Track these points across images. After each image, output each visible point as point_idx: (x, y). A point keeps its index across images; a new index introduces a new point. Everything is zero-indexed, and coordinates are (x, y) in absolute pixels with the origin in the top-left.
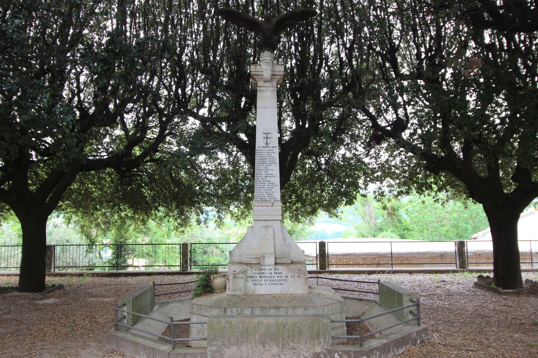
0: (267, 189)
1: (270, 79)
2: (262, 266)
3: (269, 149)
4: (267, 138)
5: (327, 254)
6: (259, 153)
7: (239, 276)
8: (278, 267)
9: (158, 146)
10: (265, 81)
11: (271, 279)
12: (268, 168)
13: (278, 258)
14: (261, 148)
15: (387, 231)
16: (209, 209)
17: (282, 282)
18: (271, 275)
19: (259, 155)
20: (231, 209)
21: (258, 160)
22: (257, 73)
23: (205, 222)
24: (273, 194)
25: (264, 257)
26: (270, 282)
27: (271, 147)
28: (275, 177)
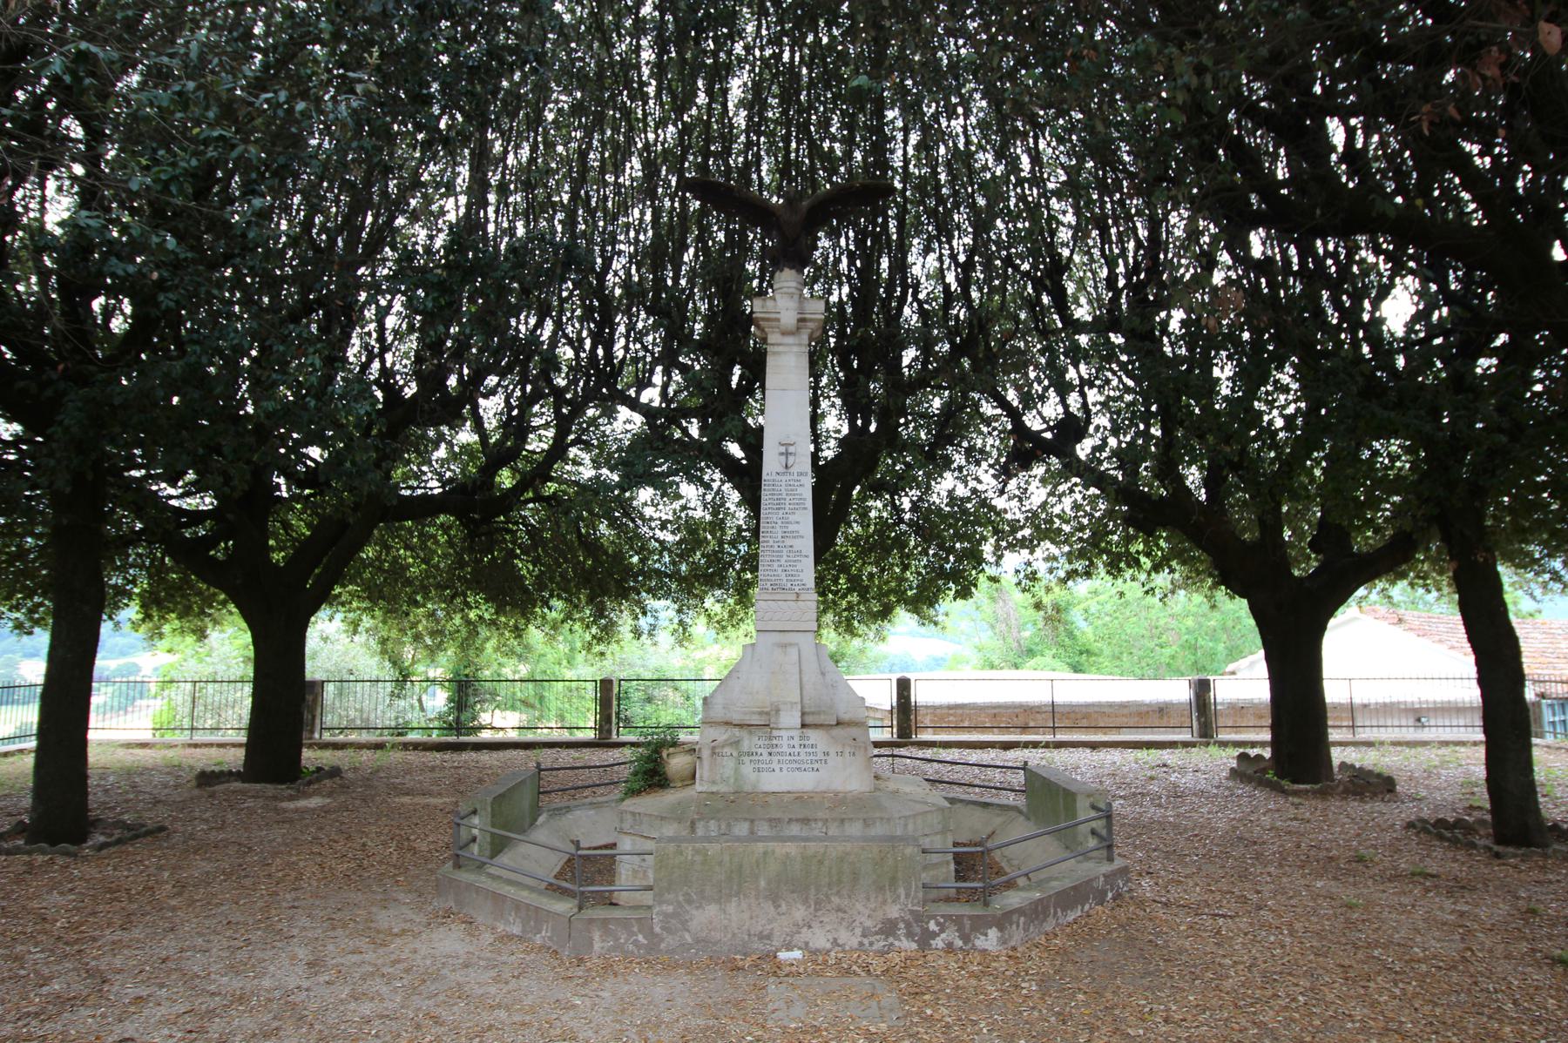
1: (794, 329)
4: (787, 454)
10: (784, 333)
11: (792, 758)
13: (809, 713)
14: (774, 477)
17: (816, 766)
18: (792, 750)
23: (650, 634)
25: (778, 711)
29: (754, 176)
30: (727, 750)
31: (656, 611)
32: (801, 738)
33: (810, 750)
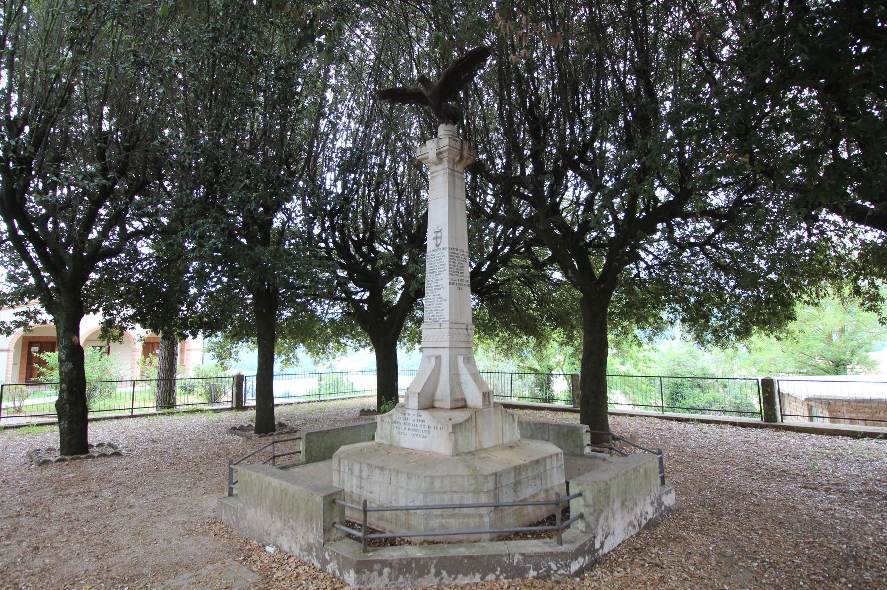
9: (509, 260)
11: (414, 428)
17: (425, 434)
29: (627, 68)
33: (421, 424)
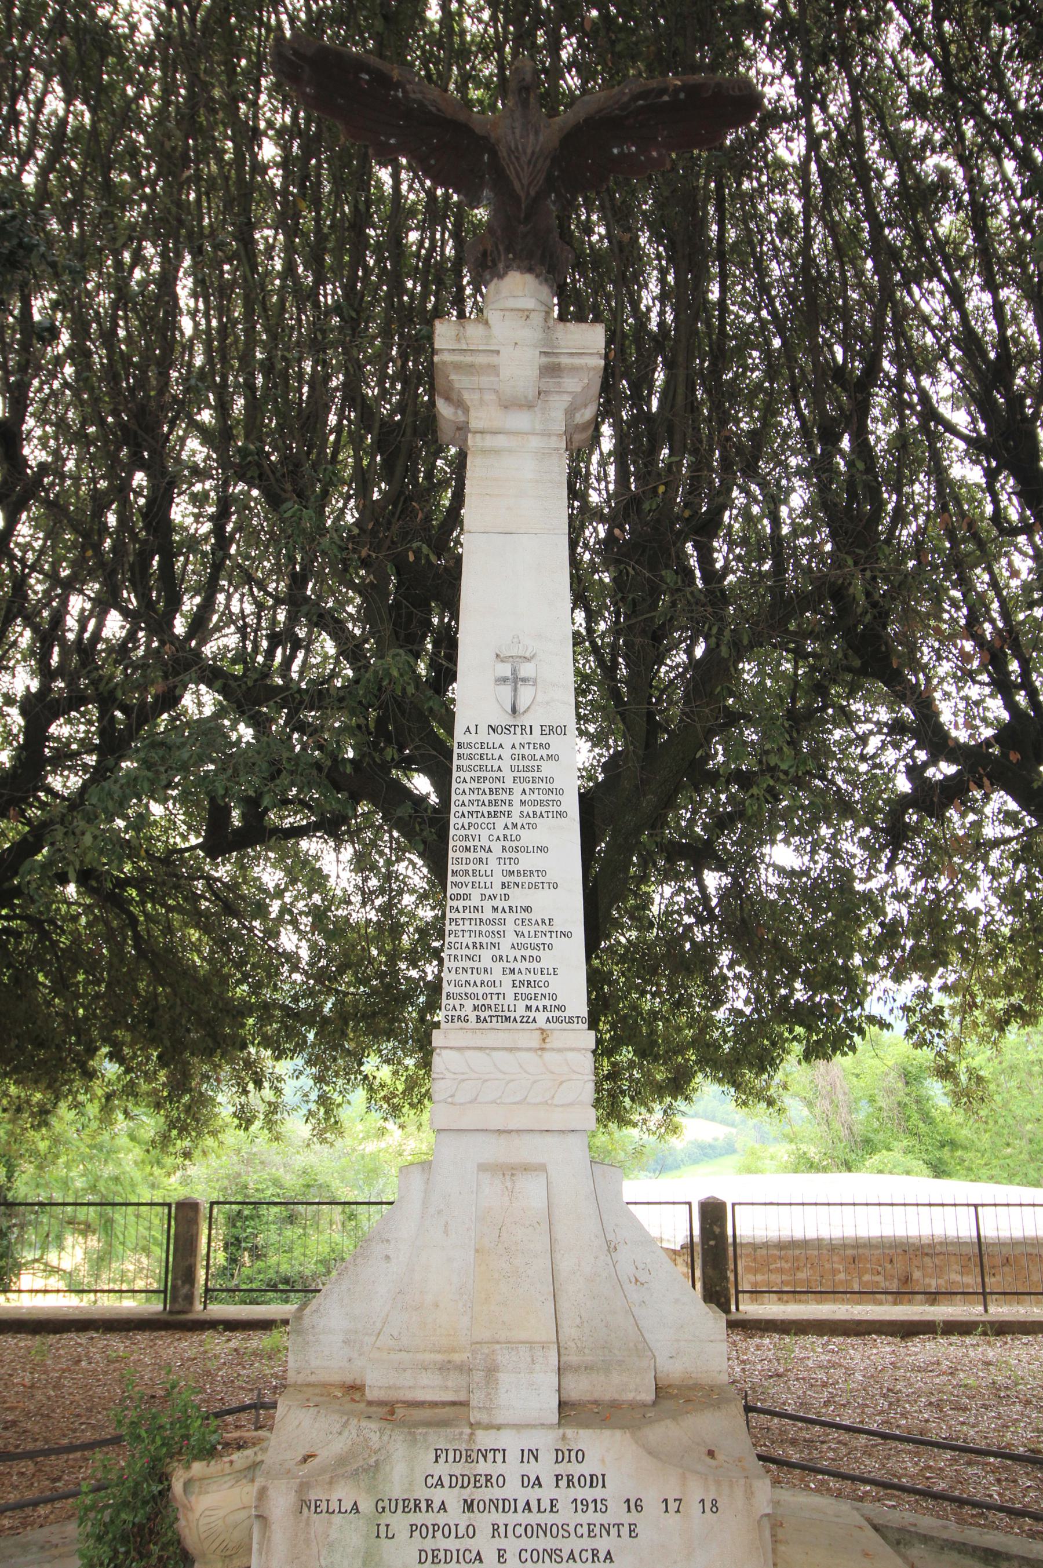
0: (512, 954)
1: (532, 393)
2: (480, 1434)
3: (526, 738)
4: (516, 681)
5: (730, 1240)
6: (471, 757)
7: (334, 1498)
8: (584, 1438)
10: (508, 404)
11: (534, 1518)
12: (518, 838)
13: (576, 1369)
14: (484, 736)
15: (889, 1150)
16: (284, 1067)
17: (603, 1544)
18: (532, 1494)
19: (470, 769)
20: (366, 1069)
21: (466, 798)
22: (468, 359)
23: (270, 1123)
24: (547, 984)
25: (491, 1371)
26: (530, 1544)
27: (537, 730)
28: (555, 886)
30: (344, 1493)
31: (279, 1079)
32: (561, 1455)
